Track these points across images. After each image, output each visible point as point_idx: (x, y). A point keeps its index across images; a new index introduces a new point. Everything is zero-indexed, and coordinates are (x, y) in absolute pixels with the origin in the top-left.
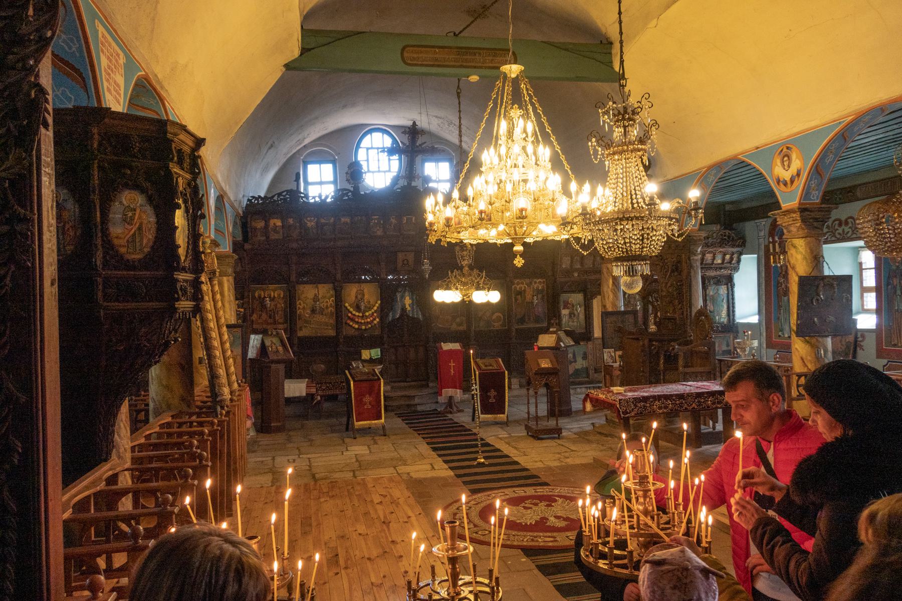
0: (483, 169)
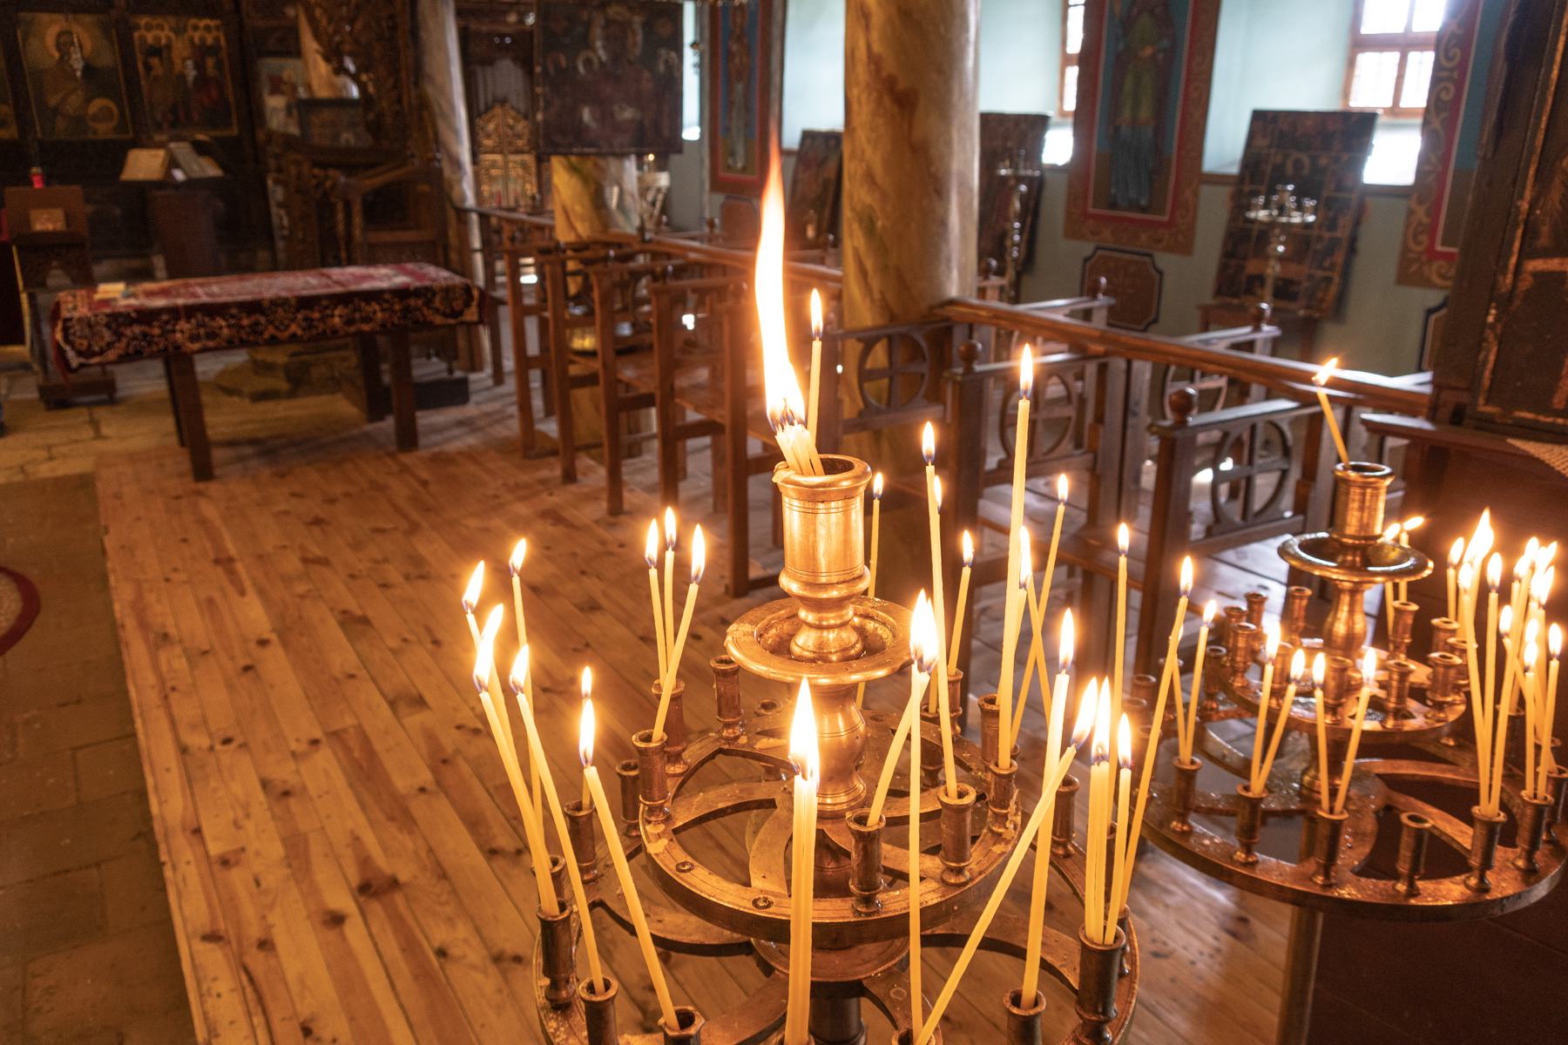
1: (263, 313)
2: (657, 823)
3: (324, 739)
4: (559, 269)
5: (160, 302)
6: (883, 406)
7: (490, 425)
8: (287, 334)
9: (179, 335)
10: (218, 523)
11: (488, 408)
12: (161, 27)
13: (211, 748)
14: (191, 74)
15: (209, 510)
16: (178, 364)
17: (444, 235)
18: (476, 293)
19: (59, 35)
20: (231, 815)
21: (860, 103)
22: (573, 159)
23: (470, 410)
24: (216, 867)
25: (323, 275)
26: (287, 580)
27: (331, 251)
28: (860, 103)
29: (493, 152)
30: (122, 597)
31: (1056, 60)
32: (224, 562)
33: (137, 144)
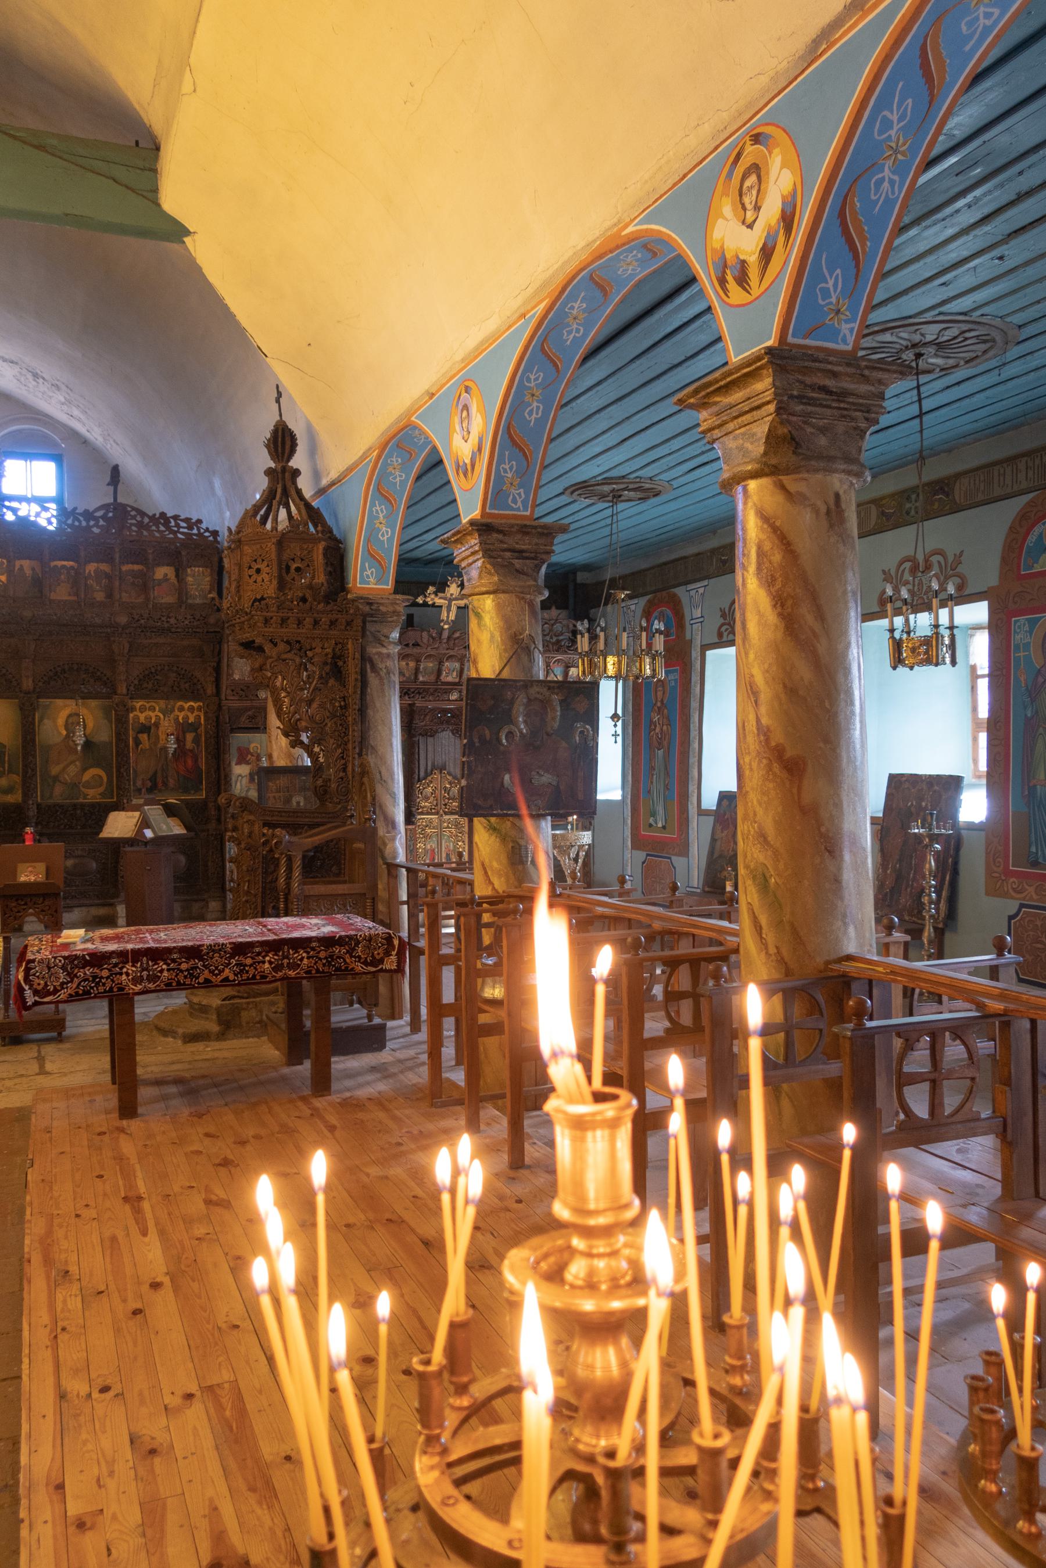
0: (219, 502)
1: (201, 959)
2: (433, 1454)
3: (198, 1394)
4: (473, 921)
5: (112, 947)
6: (781, 1061)
7: (402, 1072)
8: (220, 978)
9: (124, 977)
10: (134, 1160)
11: (401, 1055)
12: (153, 709)
13: (89, 1395)
14: (172, 746)
15: (128, 1148)
16: (120, 1004)
17: (374, 887)
18: (396, 942)
19: (70, 716)
20: (96, 1472)
21: (751, 769)
22: (493, 819)
23: (384, 1057)
24: (72, 1529)
25: (259, 923)
26: (189, 1222)
27: (271, 901)
28: (751, 769)
29: (428, 813)
30: (35, 1228)
31: (967, 725)
32: (133, 1200)
33: (118, 807)
